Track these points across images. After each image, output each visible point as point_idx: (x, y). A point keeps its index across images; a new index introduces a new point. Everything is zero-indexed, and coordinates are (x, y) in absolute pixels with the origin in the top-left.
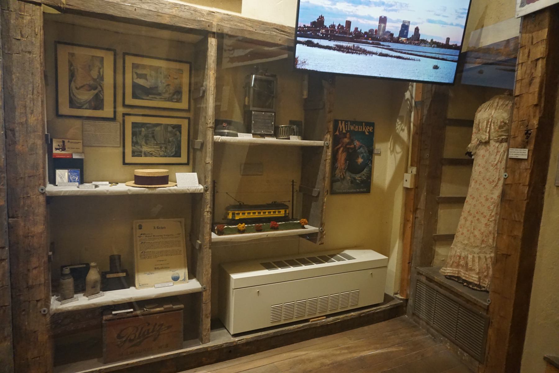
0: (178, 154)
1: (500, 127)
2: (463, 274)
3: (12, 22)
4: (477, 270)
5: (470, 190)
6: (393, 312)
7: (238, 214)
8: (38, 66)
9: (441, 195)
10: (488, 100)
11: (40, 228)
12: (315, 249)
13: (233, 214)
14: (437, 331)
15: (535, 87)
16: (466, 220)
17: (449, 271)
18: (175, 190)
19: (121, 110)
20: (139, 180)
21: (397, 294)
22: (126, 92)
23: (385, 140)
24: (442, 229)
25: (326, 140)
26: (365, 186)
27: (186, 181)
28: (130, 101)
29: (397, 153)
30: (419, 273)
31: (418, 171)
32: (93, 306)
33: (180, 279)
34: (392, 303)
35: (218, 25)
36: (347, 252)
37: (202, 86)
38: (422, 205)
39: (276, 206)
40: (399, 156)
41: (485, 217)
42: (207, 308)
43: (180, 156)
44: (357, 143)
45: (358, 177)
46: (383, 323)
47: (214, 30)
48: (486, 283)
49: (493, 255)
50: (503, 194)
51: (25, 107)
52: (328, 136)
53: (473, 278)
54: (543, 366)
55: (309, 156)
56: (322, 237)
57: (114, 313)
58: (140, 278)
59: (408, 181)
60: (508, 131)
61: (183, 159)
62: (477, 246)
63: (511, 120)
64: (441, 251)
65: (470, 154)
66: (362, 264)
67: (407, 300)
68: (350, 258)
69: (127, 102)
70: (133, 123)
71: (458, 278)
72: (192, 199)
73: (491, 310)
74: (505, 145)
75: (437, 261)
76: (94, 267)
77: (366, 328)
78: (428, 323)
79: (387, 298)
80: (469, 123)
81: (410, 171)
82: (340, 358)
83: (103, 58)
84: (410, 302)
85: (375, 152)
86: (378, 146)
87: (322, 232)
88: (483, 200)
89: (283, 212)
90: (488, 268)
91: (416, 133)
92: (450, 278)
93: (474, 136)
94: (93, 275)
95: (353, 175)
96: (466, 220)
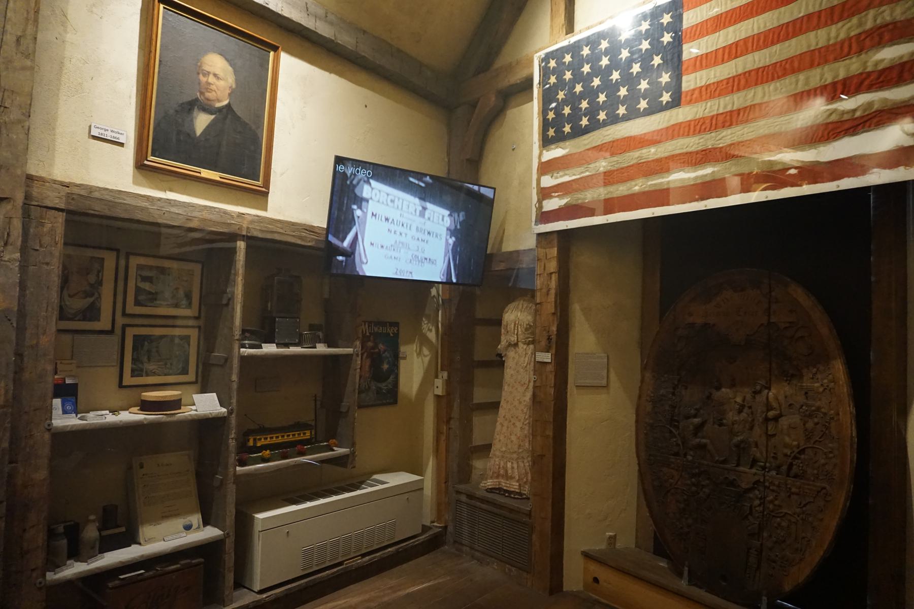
0: (185, 371)
1: (526, 330)
2: (504, 484)
3: (31, 230)
4: (517, 477)
5: (504, 394)
6: (433, 543)
7: (260, 439)
8: (56, 279)
9: (476, 401)
10: (513, 301)
11: (42, 475)
12: (343, 476)
13: (255, 440)
14: (483, 553)
15: (552, 297)
16: (502, 426)
17: (489, 483)
18: (196, 415)
19: (120, 321)
20: (146, 406)
21: (433, 522)
22: (112, 298)
23: (410, 341)
24: (478, 439)
25: (356, 347)
26: (391, 396)
27: (206, 404)
28: (131, 309)
29: (425, 356)
30: (458, 492)
31: (449, 376)
32: (97, 571)
33: (194, 527)
34: (431, 533)
35: (248, 228)
36: (375, 477)
37: (225, 292)
38: (456, 413)
39: (299, 426)
40: (427, 360)
41: (520, 421)
42: (229, 559)
43: (187, 374)
44: (381, 346)
45: (383, 387)
46: (422, 558)
47: (244, 233)
48: (526, 490)
49: (530, 459)
50: (534, 396)
51: (37, 327)
52: (358, 343)
53: (514, 486)
54: (581, 560)
55: (333, 367)
56: (354, 459)
57: (121, 577)
58: (146, 531)
59: (439, 386)
60: (533, 333)
61: (191, 377)
62: (515, 452)
63: (535, 321)
64: (478, 464)
65: (500, 356)
66: (396, 488)
67: (446, 528)
68: (383, 483)
69: (128, 311)
70: (134, 336)
71: (500, 489)
72: (207, 427)
73: (533, 514)
74: (531, 346)
75: (475, 476)
76: (94, 521)
77: (404, 566)
78: (472, 548)
79: (425, 529)
80: (498, 322)
81: (440, 376)
82: (386, 599)
83: (103, 259)
84: (450, 529)
85: (401, 355)
86: (403, 349)
87: (353, 453)
88: (516, 403)
89: (308, 433)
90: (526, 473)
91: (444, 334)
92: (491, 490)
93: (503, 338)
94: (91, 532)
95: (379, 385)
96: (502, 426)
